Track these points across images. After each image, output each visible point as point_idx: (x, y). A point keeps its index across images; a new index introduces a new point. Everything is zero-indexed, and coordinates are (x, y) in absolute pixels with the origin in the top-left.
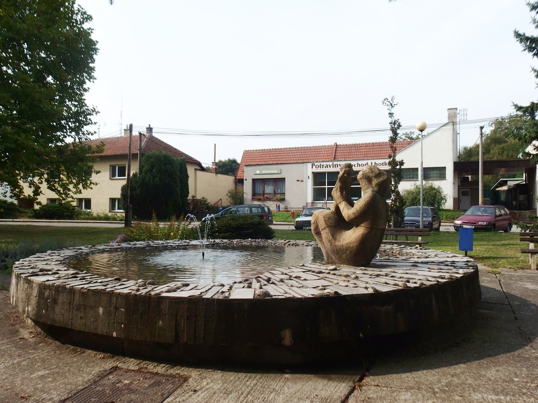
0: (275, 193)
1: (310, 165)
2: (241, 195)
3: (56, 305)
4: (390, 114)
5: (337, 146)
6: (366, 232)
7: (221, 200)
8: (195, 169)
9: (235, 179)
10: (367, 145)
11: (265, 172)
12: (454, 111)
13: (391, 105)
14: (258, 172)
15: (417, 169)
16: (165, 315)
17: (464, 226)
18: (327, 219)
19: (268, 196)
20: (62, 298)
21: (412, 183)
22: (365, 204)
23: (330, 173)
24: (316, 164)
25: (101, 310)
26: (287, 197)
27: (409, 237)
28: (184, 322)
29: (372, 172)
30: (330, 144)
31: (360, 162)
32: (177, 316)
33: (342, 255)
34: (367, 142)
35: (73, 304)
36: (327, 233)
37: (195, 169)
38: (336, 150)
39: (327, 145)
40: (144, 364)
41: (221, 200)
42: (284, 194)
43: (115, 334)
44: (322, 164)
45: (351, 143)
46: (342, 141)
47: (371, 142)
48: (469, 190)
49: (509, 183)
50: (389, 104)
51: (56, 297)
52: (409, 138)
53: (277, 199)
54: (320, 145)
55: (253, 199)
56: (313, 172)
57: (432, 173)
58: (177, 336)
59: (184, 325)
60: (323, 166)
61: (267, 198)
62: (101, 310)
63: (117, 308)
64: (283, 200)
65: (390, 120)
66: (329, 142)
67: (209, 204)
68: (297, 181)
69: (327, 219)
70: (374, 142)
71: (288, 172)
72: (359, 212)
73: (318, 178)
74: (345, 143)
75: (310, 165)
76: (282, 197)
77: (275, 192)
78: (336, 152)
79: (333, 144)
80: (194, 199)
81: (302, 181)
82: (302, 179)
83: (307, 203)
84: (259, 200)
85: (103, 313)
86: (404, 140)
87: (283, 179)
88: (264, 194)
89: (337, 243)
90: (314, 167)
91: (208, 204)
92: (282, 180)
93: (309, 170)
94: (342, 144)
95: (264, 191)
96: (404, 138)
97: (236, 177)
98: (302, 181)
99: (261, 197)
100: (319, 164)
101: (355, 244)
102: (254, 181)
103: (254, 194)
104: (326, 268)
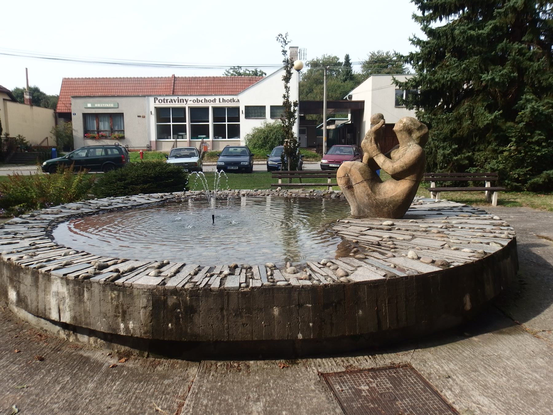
0: (112, 131)
1: (152, 99)
2: (69, 132)
3: (196, 316)
4: (283, 51)
5: (175, 78)
6: (412, 185)
7: (47, 138)
8: (4, 100)
9: (55, 113)
10: (207, 79)
11: (99, 105)
12: (295, 49)
13: (285, 42)
14: (89, 105)
15: (264, 107)
16: (365, 302)
17: (331, 165)
18: (363, 172)
19: (104, 133)
20: (203, 306)
21: (262, 121)
22: (416, 157)
23: (174, 109)
24: (159, 98)
25: (276, 311)
26: (126, 135)
27: (302, 179)
28: (385, 307)
29: (414, 124)
30: (167, 76)
31: (208, 98)
32: (377, 301)
33: (383, 208)
34: (208, 76)
35: (227, 310)
36: (365, 187)
37: (4, 100)
38: (174, 83)
39: (164, 76)
40: (352, 360)
41: (47, 138)
42: (124, 131)
43: (300, 336)
44: (166, 98)
45: (191, 76)
46: (180, 73)
47: (212, 76)
48: (305, 128)
49: (337, 122)
50: (282, 40)
51: (194, 303)
52: (236, 73)
53: (115, 137)
54: (157, 76)
55: (85, 136)
56: (155, 107)
57: (278, 111)
58: (379, 323)
59: (386, 309)
60: (167, 100)
61: (102, 136)
62: (276, 311)
63: (300, 305)
64: (123, 138)
65: (283, 58)
66: (167, 73)
67: (32, 145)
68: (138, 116)
69: (363, 172)
70: (215, 76)
71: (126, 106)
72: (408, 166)
73: (162, 114)
74: (184, 76)
75: (152, 99)
76: (121, 135)
77: (112, 129)
78: (176, 85)
79: (171, 76)
80: (8, 139)
81: (144, 117)
82: (144, 115)
83: (150, 142)
84: (94, 138)
85: (280, 314)
86: (232, 74)
87: (121, 115)
88: (98, 131)
89: (377, 197)
90: (157, 101)
91: (26, 143)
92: (121, 115)
93: (152, 104)
94: (180, 76)
95: (98, 128)
96: (232, 72)
97: (55, 110)
98: (144, 117)
99: (96, 135)
100: (162, 98)
101: (401, 198)
102: (85, 115)
103: (86, 131)
104: (381, 223)
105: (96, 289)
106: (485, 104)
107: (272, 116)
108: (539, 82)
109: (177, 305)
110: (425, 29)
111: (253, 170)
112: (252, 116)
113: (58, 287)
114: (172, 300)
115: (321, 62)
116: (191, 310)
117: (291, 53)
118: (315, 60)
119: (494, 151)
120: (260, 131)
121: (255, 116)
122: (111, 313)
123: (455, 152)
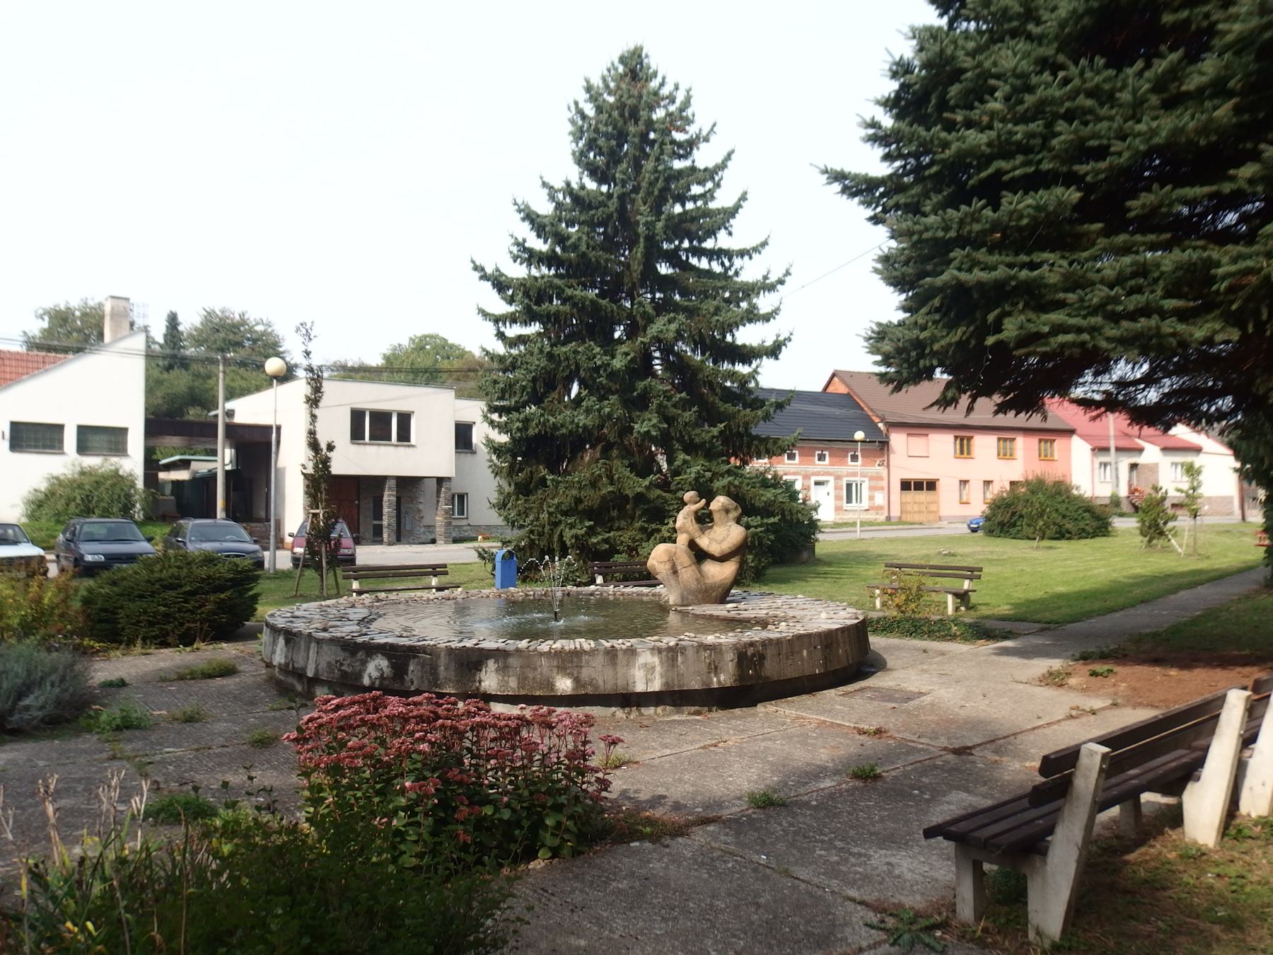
15: (59, 428)
25: (805, 653)
62: (805, 653)
105: (690, 653)
106: (626, 462)
107: (82, 448)
108: (690, 436)
109: (753, 655)
110: (501, 335)
111: (820, 549)
112: (29, 446)
113: (897, 600)
114: (750, 651)
115: (78, 313)
116: (762, 657)
117: (112, 308)
118: (63, 308)
119: (642, 530)
120: (57, 482)
121: (36, 447)
122: (705, 670)
123: (591, 531)
